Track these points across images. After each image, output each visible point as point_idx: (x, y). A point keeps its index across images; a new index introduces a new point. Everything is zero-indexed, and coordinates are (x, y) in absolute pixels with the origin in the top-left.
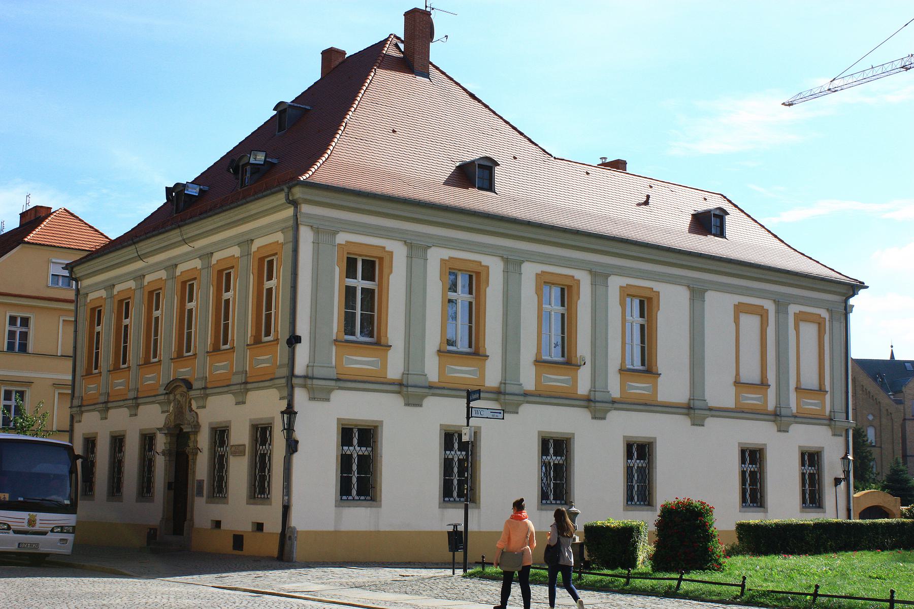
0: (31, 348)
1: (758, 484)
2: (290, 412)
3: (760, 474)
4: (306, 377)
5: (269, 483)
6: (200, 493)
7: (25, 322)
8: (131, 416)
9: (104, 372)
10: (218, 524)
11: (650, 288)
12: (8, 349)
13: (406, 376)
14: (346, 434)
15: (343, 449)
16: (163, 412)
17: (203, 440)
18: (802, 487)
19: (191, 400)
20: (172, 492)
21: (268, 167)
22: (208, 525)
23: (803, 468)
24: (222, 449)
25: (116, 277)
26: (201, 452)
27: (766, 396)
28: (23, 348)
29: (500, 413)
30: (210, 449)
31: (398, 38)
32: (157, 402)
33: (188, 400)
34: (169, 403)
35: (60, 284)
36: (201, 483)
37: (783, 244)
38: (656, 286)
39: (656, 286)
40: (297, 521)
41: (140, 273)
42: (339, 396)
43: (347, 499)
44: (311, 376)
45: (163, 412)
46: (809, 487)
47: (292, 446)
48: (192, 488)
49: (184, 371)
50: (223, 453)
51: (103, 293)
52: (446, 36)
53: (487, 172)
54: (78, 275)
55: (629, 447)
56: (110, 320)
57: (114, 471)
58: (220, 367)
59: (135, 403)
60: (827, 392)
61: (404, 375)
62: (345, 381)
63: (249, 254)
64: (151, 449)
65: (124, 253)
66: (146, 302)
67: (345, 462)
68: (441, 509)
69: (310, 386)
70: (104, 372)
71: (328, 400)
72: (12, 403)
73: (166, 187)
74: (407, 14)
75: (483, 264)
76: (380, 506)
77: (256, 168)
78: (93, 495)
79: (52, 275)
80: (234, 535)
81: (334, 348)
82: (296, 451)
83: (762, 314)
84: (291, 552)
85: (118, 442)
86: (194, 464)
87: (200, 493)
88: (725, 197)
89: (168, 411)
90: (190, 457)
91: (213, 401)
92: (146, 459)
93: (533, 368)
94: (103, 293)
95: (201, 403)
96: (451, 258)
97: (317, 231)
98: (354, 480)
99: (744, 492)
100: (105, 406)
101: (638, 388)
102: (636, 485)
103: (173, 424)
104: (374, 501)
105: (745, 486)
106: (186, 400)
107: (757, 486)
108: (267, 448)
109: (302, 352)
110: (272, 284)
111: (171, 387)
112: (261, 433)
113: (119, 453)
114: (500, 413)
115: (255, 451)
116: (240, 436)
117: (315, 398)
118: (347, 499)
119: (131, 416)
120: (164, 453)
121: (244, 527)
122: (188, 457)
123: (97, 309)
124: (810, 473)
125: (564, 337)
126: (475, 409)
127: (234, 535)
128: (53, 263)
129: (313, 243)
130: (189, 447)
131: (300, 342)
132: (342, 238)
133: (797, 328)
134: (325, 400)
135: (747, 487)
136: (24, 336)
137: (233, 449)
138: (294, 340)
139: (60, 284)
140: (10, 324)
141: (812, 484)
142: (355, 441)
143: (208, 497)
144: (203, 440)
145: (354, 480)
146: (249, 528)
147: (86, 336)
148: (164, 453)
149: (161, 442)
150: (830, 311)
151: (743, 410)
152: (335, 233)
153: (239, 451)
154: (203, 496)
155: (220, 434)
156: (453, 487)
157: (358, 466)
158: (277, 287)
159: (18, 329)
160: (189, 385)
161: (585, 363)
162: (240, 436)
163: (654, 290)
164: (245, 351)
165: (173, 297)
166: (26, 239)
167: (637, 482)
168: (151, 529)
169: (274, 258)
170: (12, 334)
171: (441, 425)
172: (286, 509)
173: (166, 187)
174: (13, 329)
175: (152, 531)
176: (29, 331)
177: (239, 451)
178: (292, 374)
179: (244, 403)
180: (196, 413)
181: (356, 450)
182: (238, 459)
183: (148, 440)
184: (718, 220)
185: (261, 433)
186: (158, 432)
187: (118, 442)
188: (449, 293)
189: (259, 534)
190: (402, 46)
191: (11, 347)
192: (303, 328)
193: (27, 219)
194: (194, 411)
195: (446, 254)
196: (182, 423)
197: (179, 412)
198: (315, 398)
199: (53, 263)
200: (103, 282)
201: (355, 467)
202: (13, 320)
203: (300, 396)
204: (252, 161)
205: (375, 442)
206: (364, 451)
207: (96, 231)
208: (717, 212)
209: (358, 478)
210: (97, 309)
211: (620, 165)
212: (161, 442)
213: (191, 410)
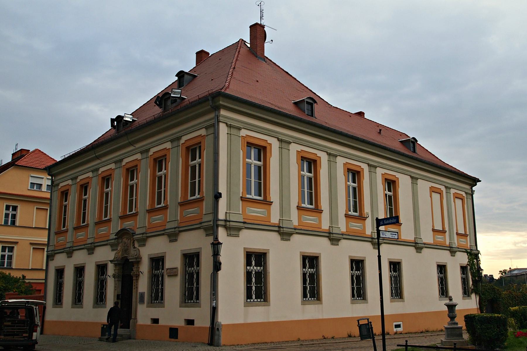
0: (17, 224)
2: (216, 245)
4: (226, 221)
5: (440, 292)
6: (142, 301)
7: (15, 208)
12: (5, 223)
13: (282, 221)
15: (247, 268)
17: (145, 267)
18: (352, 286)
19: (134, 240)
24: (81, 278)
26: (142, 274)
27: (445, 236)
28: (13, 223)
29: (396, 235)
30: (149, 272)
32: (108, 244)
33: (132, 241)
35: (35, 188)
36: (142, 295)
38: (398, 175)
39: (398, 175)
40: (223, 319)
44: (229, 220)
46: (356, 286)
47: (217, 266)
48: (135, 298)
49: (128, 224)
50: (81, 281)
52: (272, 40)
54: (53, 173)
56: (75, 197)
57: (57, 290)
60: (468, 235)
61: (280, 220)
68: (302, 306)
69: (229, 226)
71: (238, 236)
72: (7, 253)
73: (111, 119)
74: (251, 27)
76: (269, 305)
78: (62, 304)
79: (31, 183)
81: (241, 202)
82: (220, 270)
83: (440, 193)
84: (219, 339)
86: (137, 282)
87: (142, 301)
89: (117, 249)
90: (134, 278)
92: (59, 283)
93: (345, 218)
97: (229, 126)
98: (254, 288)
99: (305, 289)
102: (308, 286)
103: (121, 257)
104: (318, 300)
105: (354, 286)
106: (131, 242)
107: (360, 286)
108: (104, 278)
109: (223, 203)
111: (122, 233)
113: (60, 279)
114: (396, 235)
121: (179, 323)
123: (65, 192)
126: (382, 232)
128: (32, 176)
129: (227, 134)
130: (133, 271)
131: (221, 198)
132: (244, 133)
133: (454, 202)
135: (355, 286)
136: (14, 216)
137: (168, 271)
138: (218, 196)
139: (35, 188)
140: (6, 210)
141: (358, 283)
143: (148, 303)
144: (145, 267)
145: (254, 288)
146: (182, 323)
149: (111, 270)
150: (466, 193)
151: (437, 244)
152: (239, 129)
153: (173, 273)
156: (252, 291)
159: (11, 212)
161: (368, 216)
165: (120, 178)
166: (16, 163)
167: (309, 284)
170: (7, 215)
171: (300, 252)
172: (214, 310)
173: (111, 119)
174: (8, 212)
175: (105, 326)
176: (17, 214)
177: (173, 273)
178: (216, 219)
180: (138, 249)
181: (254, 268)
183: (101, 268)
186: (110, 262)
191: (6, 222)
192: (222, 189)
193: (16, 156)
194: (136, 248)
195: (300, 148)
196: (128, 256)
197: (126, 250)
199: (32, 176)
202: (8, 208)
203: (222, 233)
205: (265, 263)
208: (413, 140)
210: (65, 192)
211: (362, 114)
212: (111, 270)
213: (135, 248)
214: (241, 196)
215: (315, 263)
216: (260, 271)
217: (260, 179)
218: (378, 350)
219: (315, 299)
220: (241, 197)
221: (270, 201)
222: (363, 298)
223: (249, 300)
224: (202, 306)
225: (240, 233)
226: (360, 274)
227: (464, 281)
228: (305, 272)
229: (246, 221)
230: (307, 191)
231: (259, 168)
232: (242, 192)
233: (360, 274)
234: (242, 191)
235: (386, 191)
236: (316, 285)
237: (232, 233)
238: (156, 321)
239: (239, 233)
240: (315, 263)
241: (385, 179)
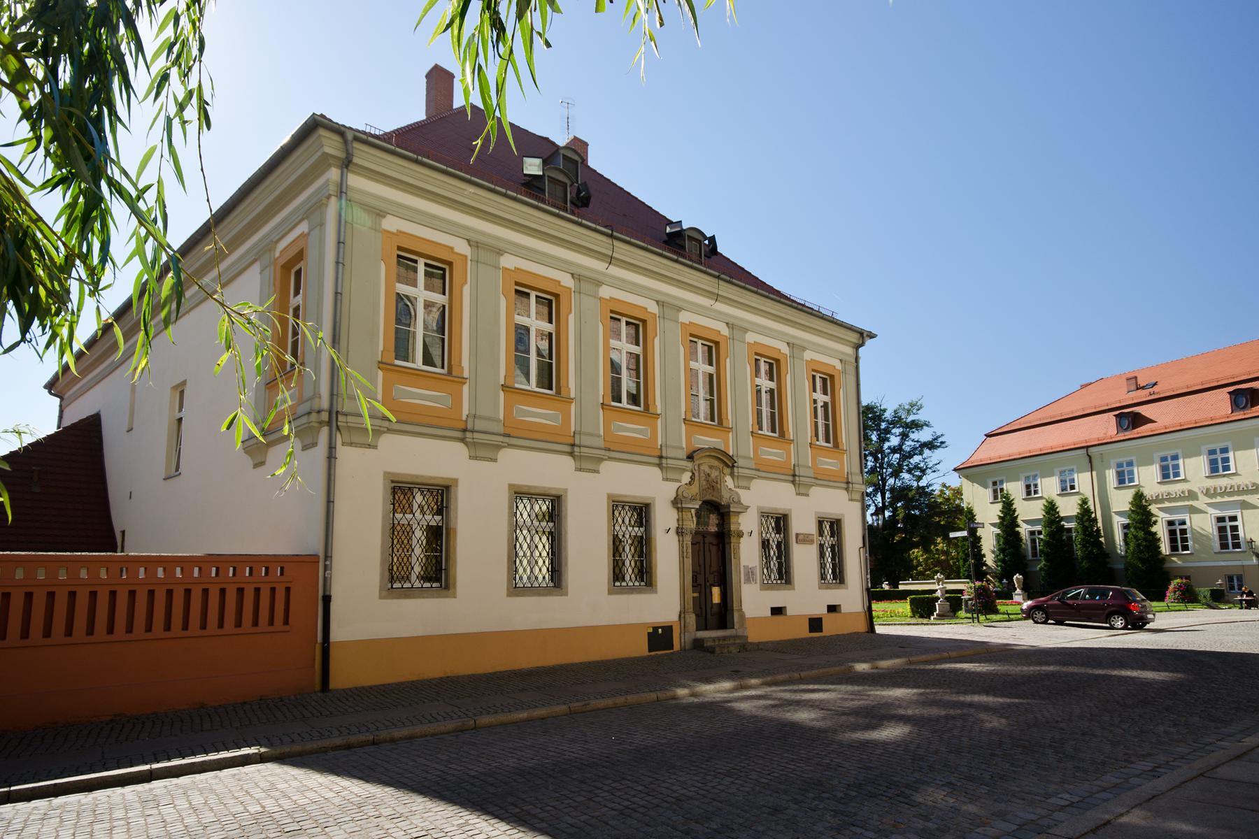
1: (783, 558)
3: (838, 547)
11: (717, 331)
23: (821, 538)
42: (508, 456)
43: (432, 587)
62: (617, 450)
65: (286, 227)
75: (456, 250)
80: (809, 619)
81: (502, 394)
96: (400, 232)
101: (775, 455)
104: (557, 587)
116: (802, 523)
117: (352, 443)
118: (432, 587)
121: (821, 611)
125: (640, 382)
127: (809, 619)
134: (368, 446)
146: (825, 611)
163: (782, 351)
164: (848, 449)
177: (804, 539)
188: (398, 285)
198: (352, 443)
214: (503, 383)
215: (782, 525)
216: (639, 534)
217: (711, 394)
218: (8, 808)
219: (783, 581)
220: (502, 385)
221: (459, 375)
222: (840, 580)
223: (618, 584)
224: (509, 598)
225: (751, 484)
226: (834, 543)
227: (397, 536)
228: (823, 542)
229: (758, 467)
230: (767, 411)
231: (711, 376)
232: (686, 412)
233: (834, 543)
234: (684, 410)
235: (771, 391)
236: (783, 560)
237: (481, 453)
238: (777, 611)
239: (497, 454)
240: (782, 525)
241: (425, 275)
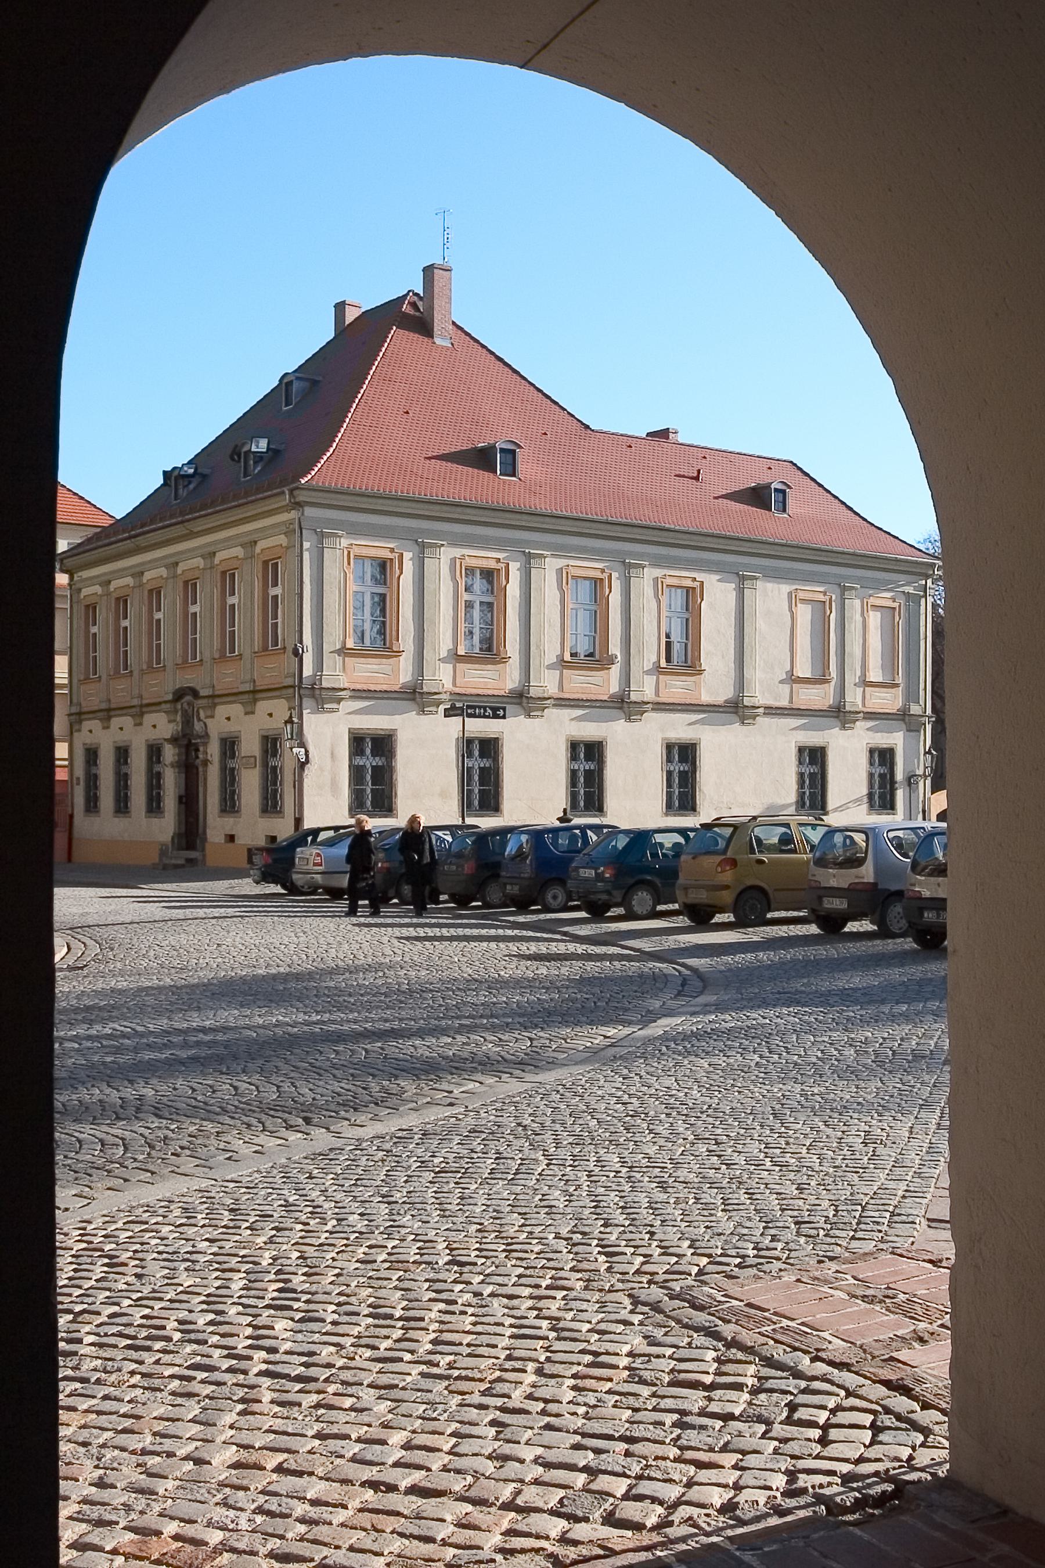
8: (136, 725)
9: (104, 677)
10: (231, 838)
14: (357, 741)
16: (170, 722)
17: (213, 750)
20: (183, 806)
21: (273, 453)
22: (220, 839)
25: (111, 573)
31: (417, 295)
34: (176, 712)
37: (858, 518)
39: (700, 576)
41: (138, 569)
45: (170, 722)
51: (98, 589)
53: (510, 456)
55: (669, 747)
58: (228, 678)
59: (139, 711)
63: (253, 556)
64: (159, 762)
66: (146, 602)
67: (356, 774)
70: (104, 677)
77: (259, 457)
85: (122, 754)
88: (795, 465)
89: (174, 721)
90: (201, 769)
91: (222, 711)
94: (98, 589)
95: (209, 713)
98: (369, 791)
100: (107, 714)
110: (277, 591)
111: (179, 695)
112: (271, 745)
115: (265, 764)
116: (250, 746)
119: (136, 725)
120: (172, 765)
122: (197, 768)
124: (810, 773)
142: (368, 751)
144: (213, 750)
147: (82, 639)
148: (172, 765)
149: (170, 753)
154: (504, 660)
155: (229, 745)
157: (372, 777)
158: (283, 595)
160: (195, 693)
162: (250, 746)
168: (162, 845)
169: (279, 561)
179: (253, 713)
182: (250, 771)
183: (154, 752)
184: (781, 495)
185: (271, 745)
187: (122, 754)
189: (230, 845)
190: (420, 304)
200: (98, 576)
201: (368, 777)
204: (254, 449)
206: (378, 761)
207: (82, 498)
209: (372, 790)
212: (170, 753)
213: (199, 720)
